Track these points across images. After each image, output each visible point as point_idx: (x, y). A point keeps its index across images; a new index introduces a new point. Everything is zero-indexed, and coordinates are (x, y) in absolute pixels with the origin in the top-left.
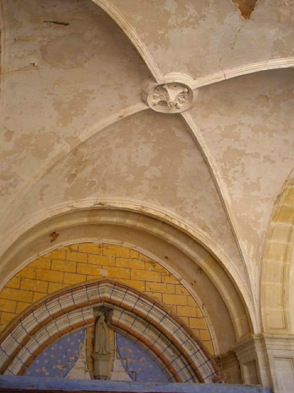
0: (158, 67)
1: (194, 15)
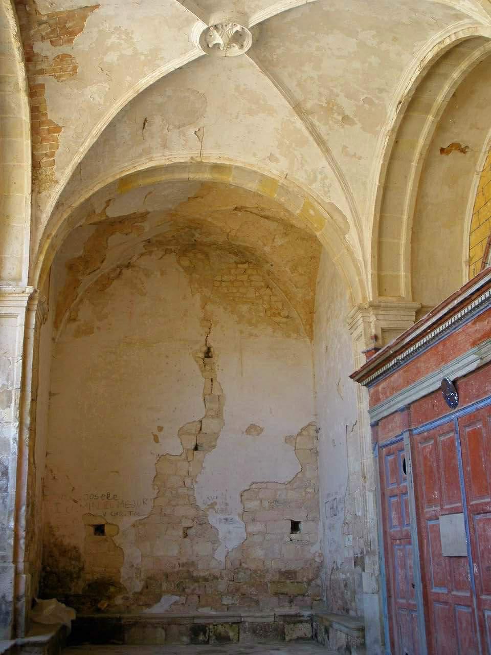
0: (185, 53)
1: (118, 36)
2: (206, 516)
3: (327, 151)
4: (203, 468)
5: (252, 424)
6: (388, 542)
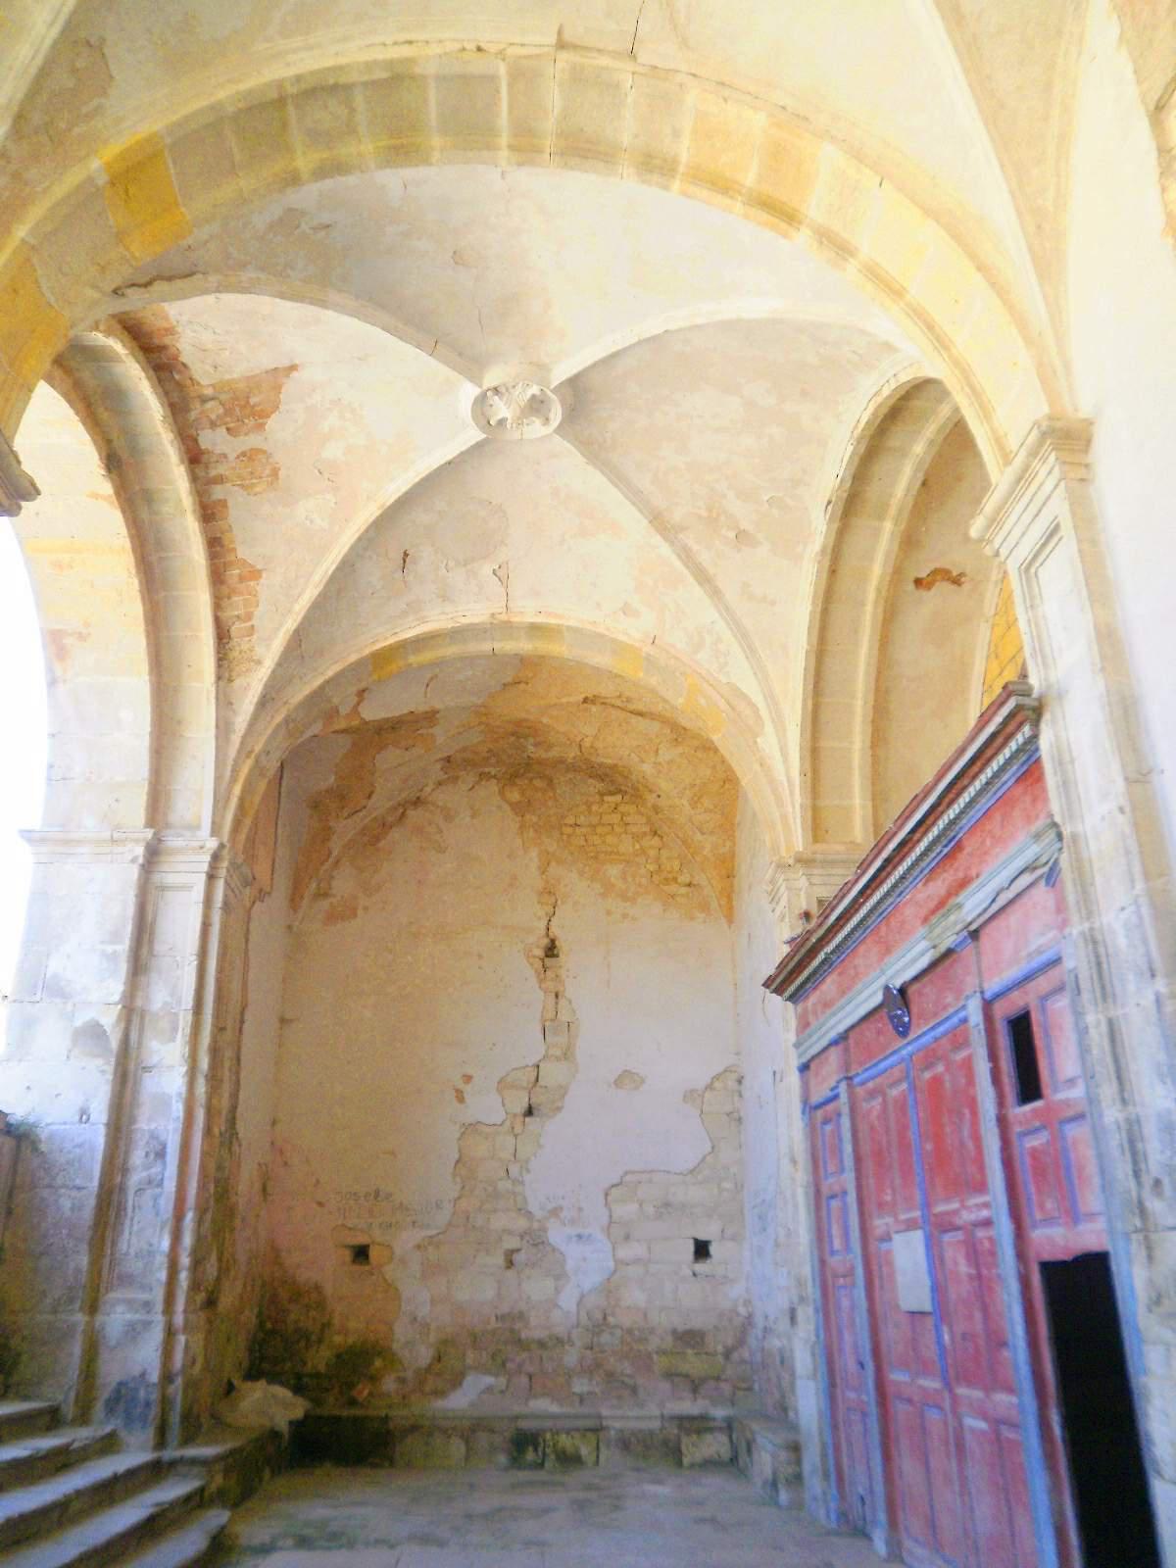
2: (544, 1230)
3: (716, 594)
4: (540, 1146)
5: (626, 1071)
6: (826, 1284)
